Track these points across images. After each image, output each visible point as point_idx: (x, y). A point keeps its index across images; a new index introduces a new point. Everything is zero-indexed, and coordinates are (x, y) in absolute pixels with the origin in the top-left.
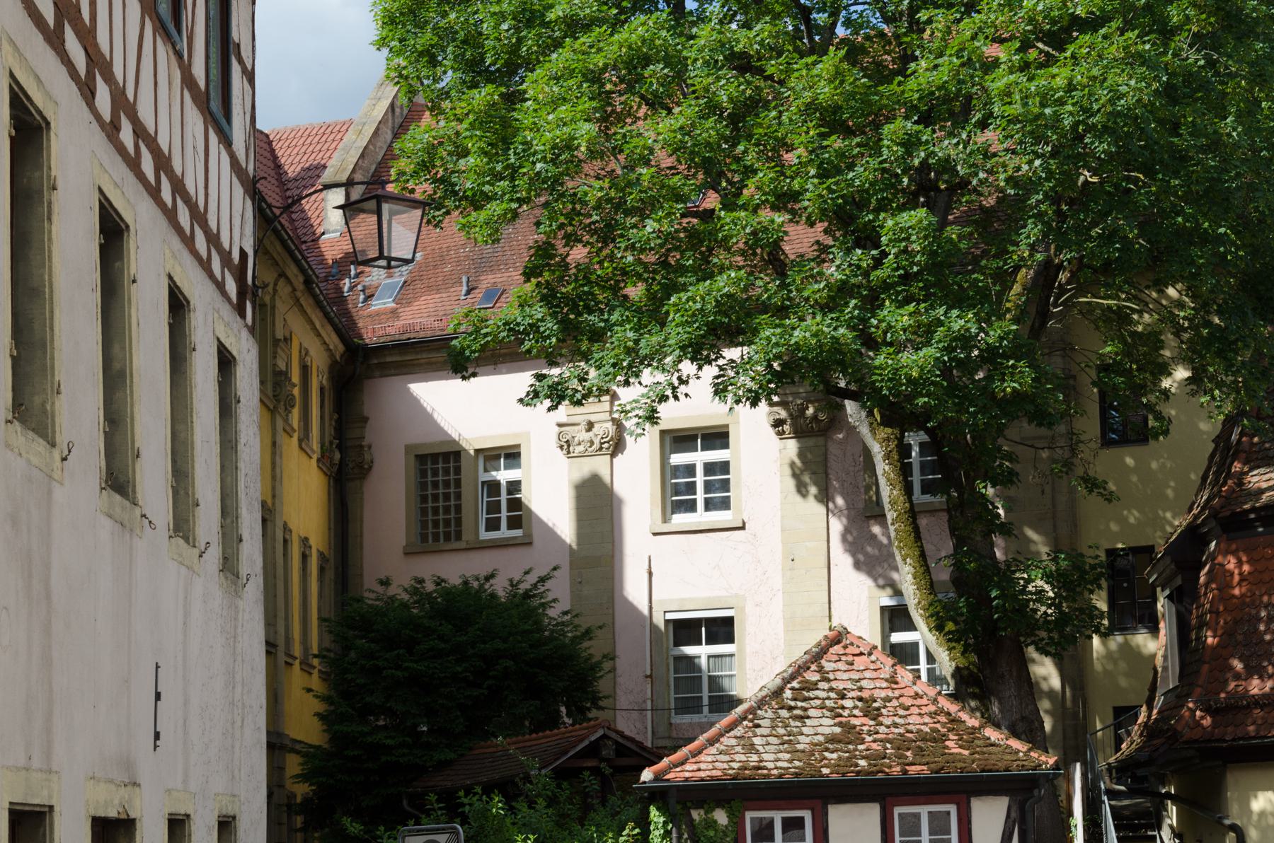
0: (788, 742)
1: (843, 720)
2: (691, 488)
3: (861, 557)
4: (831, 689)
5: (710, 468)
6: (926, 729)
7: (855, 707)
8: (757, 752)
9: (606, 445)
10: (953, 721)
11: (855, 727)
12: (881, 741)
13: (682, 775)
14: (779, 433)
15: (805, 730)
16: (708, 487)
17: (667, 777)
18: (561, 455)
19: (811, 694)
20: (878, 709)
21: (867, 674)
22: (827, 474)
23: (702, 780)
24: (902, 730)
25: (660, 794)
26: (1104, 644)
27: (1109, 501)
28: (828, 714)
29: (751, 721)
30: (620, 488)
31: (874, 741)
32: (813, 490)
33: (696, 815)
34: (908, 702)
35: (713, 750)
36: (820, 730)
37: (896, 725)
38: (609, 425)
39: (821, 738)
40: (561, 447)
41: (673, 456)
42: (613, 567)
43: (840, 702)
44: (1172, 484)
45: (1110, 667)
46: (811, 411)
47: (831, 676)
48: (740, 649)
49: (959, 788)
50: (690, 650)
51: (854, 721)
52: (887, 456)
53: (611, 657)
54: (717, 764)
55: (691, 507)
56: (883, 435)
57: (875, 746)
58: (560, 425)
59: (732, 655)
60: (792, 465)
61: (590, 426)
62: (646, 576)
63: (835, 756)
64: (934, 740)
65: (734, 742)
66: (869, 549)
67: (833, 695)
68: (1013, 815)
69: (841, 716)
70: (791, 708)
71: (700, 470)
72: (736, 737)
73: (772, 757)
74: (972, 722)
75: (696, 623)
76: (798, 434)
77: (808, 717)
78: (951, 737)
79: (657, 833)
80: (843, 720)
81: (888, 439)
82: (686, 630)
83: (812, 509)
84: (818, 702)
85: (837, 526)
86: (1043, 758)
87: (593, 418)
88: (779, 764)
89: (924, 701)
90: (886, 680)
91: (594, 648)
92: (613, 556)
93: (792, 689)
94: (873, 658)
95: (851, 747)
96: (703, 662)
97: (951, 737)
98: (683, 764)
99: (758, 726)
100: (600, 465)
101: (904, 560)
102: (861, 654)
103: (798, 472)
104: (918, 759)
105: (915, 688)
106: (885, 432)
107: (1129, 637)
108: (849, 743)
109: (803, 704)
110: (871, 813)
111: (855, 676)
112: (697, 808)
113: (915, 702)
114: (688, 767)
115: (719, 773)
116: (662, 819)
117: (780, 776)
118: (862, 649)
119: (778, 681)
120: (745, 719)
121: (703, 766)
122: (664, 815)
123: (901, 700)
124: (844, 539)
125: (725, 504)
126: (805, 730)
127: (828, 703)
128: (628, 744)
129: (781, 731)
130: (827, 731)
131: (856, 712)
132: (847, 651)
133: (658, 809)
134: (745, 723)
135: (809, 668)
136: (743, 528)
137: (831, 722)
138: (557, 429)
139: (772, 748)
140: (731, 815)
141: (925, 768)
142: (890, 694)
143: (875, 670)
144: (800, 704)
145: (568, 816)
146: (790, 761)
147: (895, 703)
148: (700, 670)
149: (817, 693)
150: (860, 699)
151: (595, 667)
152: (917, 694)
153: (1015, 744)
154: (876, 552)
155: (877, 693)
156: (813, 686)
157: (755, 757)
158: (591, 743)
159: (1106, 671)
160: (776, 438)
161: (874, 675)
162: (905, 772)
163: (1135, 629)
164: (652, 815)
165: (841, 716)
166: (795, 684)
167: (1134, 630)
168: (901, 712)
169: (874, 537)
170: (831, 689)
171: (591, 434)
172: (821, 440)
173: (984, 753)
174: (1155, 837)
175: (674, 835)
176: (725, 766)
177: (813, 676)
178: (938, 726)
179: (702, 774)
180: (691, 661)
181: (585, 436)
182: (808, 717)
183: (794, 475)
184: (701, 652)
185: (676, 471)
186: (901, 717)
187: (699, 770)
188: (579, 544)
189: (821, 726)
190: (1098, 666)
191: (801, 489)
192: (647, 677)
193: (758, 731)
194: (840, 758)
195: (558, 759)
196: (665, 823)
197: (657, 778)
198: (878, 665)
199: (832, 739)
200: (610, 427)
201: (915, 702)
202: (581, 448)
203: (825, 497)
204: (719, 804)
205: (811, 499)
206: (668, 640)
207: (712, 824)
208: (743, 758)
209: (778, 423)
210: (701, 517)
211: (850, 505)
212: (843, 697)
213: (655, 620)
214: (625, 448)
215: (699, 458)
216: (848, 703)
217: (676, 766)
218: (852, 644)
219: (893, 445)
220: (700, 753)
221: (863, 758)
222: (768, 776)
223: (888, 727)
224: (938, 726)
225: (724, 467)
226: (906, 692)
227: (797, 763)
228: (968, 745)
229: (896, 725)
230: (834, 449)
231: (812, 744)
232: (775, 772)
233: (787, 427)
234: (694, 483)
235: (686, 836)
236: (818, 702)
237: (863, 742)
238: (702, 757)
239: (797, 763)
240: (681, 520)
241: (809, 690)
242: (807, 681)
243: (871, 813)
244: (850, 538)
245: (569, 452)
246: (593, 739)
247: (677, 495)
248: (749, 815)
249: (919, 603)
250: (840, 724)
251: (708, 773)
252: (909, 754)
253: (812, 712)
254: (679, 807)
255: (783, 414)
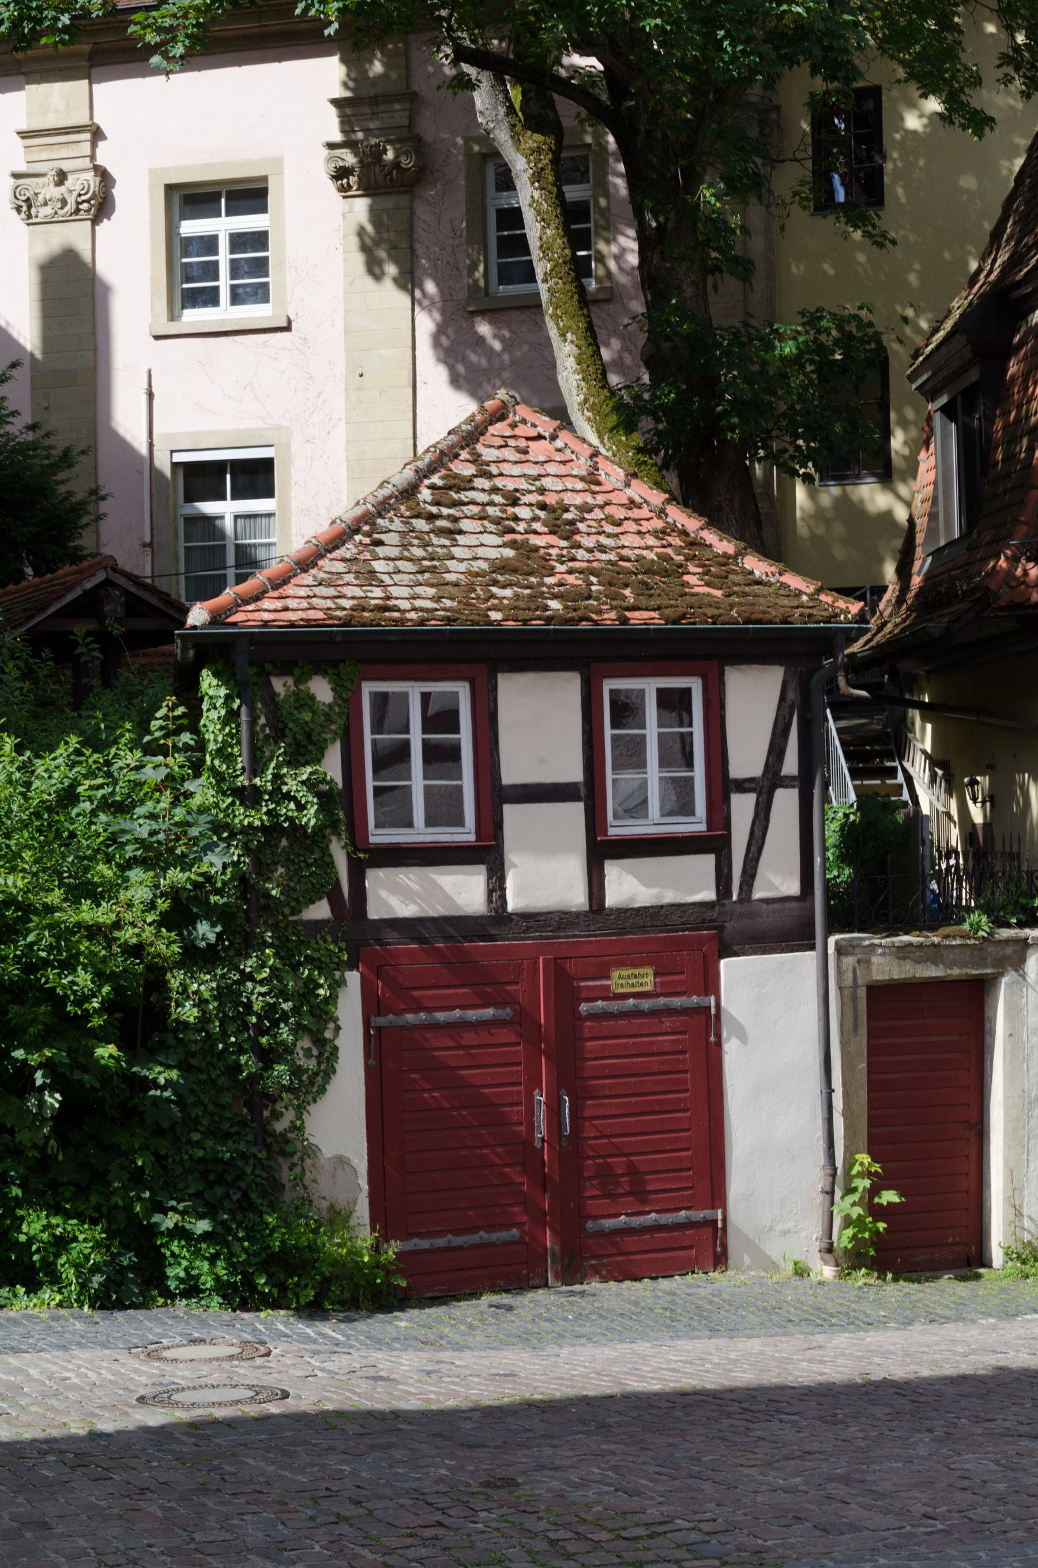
0: (431, 569)
1: (518, 537)
2: (211, 271)
3: (461, 369)
4: (495, 490)
5: (239, 242)
6: (651, 556)
7: (536, 519)
8: (381, 584)
9: (85, 206)
10: (693, 544)
11: (536, 549)
12: (581, 572)
13: (256, 616)
14: (342, 189)
15: (456, 551)
16: (236, 268)
17: (231, 619)
18: (17, 220)
19: (463, 496)
20: (572, 523)
21: (552, 469)
22: (412, 250)
23: (292, 625)
24: (612, 557)
25: (220, 649)
26: (812, 495)
27: (880, 245)
28: (492, 528)
29: (368, 535)
30: (105, 268)
31: (570, 572)
32: (391, 270)
33: (280, 686)
34: (620, 513)
35: (307, 579)
36: (481, 552)
37: (602, 548)
38: (90, 175)
39: (484, 566)
40: (18, 209)
41: (184, 223)
42: (95, 386)
43: (511, 510)
44: (917, 267)
45: (820, 531)
46: (390, 155)
47: (494, 469)
48: (284, 506)
49: (706, 649)
50: (209, 507)
51: (535, 540)
52: (537, 177)
53: (96, 494)
54: (315, 601)
55: (210, 298)
56: (531, 144)
57: (571, 579)
58: (16, 176)
59: (270, 515)
60: (361, 232)
61: (61, 177)
62: (144, 398)
63: (508, 592)
64: (666, 573)
65: (340, 567)
66: (473, 358)
67: (498, 499)
68: (791, 696)
69: (513, 531)
70: (431, 517)
71: (224, 245)
72: (343, 560)
73: (405, 592)
74: (722, 545)
75: (219, 467)
76: (368, 189)
77: (461, 532)
78: (692, 568)
79: (214, 715)
80: (518, 537)
81: (538, 151)
82: (203, 478)
83: (390, 298)
84: (475, 509)
85: (426, 324)
86: (841, 604)
87: (66, 166)
88: (418, 603)
89: (645, 513)
90: (582, 479)
91: (72, 484)
92: (95, 370)
93: (432, 487)
94: (559, 443)
95: (533, 580)
96: (228, 524)
97: (692, 568)
98: (257, 598)
99: (380, 543)
100: (76, 235)
101: (563, 335)
102: (540, 437)
103: (368, 242)
104: (643, 601)
105: (629, 492)
106: (533, 140)
107: (849, 488)
108: (530, 574)
109: (451, 511)
110: (566, 689)
111: (533, 470)
112: (280, 674)
113: (630, 514)
114: (266, 604)
115: (320, 615)
116: (223, 691)
117: (422, 622)
118: (540, 430)
119: (409, 474)
120: (357, 531)
121: (292, 603)
122: (226, 683)
123: (608, 510)
124: (436, 342)
125: (261, 294)
126: (456, 551)
127: (491, 510)
128: (146, 596)
129: (419, 552)
130: (493, 553)
131: (537, 526)
132: (518, 431)
133: (216, 674)
134: (358, 538)
135: (456, 456)
136: (287, 328)
137: (497, 540)
138: (12, 182)
139: (406, 579)
140: (338, 688)
141: (655, 614)
142: (589, 499)
143: (563, 463)
144: (445, 511)
145: (52, 703)
146: (437, 599)
147: (598, 514)
148: (222, 535)
149: (472, 495)
150: (543, 506)
151: (79, 509)
152: (632, 501)
153: (794, 581)
154: (484, 362)
155: (568, 499)
156: (466, 484)
157: (378, 592)
158: (86, 592)
159: (813, 536)
160: (337, 196)
161: (563, 470)
162: (625, 621)
163: (858, 477)
164: (204, 685)
165: (513, 531)
166: (436, 479)
167: (856, 478)
168: (609, 529)
169: (481, 340)
170: (495, 490)
171: (62, 189)
172: (404, 200)
173: (747, 595)
174: (895, 769)
175: (244, 718)
176: (329, 604)
177: (464, 469)
178: (669, 551)
179: (292, 616)
180: (210, 522)
181: (54, 192)
182: (461, 532)
183: (364, 248)
184: (225, 509)
185: (189, 245)
186: (609, 536)
187: (286, 609)
188: (44, 352)
189: (480, 547)
190: (802, 530)
191: (374, 268)
192: (145, 545)
193: (380, 551)
194: (517, 596)
195: (33, 616)
196: (228, 697)
197: (217, 619)
198: (568, 455)
199: (501, 567)
200: (90, 178)
201: (630, 514)
202: (47, 211)
203: (408, 281)
204: (319, 669)
205: (388, 284)
206: (175, 489)
207: (307, 701)
208: (358, 592)
209: (340, 174)
210: (224, 313)
211: (446, 295)
212: (515, 503)
213: (157, 463)
214: (112, 210)
215: (222, 226)
216: (524, 512)
217: (247, 602)
218: (524, 421)
219: (545, 160)
220: (285, 582)
221: (555, 597)
222: (402, 621)
223: (590, 551)
224: (669, 551)
225: (259, 240)
226: (614, 497)
227: (448, 603)
228: (718, 581)
229: (602, 548)
230: (423, 213)
231: (469, 573)
232: (413, 615)
233: (353, 180)
234: (216, 263)
235: (262, 721)
236: (475, 509)
237: (552, 572)
238: (289, 590)
239: (448, 603)
240: (195, 317)
241: (459, 490)
242: (456, 476)
243: (566, 689)
244: (444, 341)
245: (29, 217)
246: (89, 585)
247: (190, 283)
248: (368, 688)
249: (586, 401)
250: (512, 544)
251: (301, 614)
252: (627, 592)
253: (465, 525)
254: (252, 671)
255: (349, 159)
